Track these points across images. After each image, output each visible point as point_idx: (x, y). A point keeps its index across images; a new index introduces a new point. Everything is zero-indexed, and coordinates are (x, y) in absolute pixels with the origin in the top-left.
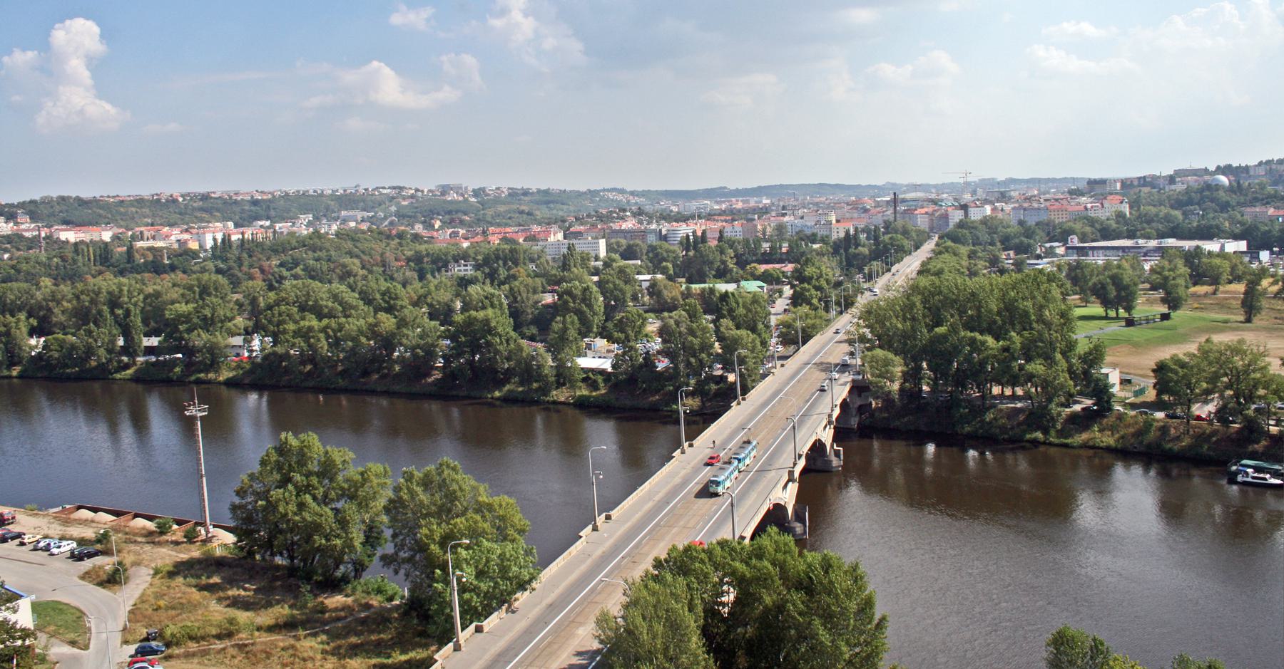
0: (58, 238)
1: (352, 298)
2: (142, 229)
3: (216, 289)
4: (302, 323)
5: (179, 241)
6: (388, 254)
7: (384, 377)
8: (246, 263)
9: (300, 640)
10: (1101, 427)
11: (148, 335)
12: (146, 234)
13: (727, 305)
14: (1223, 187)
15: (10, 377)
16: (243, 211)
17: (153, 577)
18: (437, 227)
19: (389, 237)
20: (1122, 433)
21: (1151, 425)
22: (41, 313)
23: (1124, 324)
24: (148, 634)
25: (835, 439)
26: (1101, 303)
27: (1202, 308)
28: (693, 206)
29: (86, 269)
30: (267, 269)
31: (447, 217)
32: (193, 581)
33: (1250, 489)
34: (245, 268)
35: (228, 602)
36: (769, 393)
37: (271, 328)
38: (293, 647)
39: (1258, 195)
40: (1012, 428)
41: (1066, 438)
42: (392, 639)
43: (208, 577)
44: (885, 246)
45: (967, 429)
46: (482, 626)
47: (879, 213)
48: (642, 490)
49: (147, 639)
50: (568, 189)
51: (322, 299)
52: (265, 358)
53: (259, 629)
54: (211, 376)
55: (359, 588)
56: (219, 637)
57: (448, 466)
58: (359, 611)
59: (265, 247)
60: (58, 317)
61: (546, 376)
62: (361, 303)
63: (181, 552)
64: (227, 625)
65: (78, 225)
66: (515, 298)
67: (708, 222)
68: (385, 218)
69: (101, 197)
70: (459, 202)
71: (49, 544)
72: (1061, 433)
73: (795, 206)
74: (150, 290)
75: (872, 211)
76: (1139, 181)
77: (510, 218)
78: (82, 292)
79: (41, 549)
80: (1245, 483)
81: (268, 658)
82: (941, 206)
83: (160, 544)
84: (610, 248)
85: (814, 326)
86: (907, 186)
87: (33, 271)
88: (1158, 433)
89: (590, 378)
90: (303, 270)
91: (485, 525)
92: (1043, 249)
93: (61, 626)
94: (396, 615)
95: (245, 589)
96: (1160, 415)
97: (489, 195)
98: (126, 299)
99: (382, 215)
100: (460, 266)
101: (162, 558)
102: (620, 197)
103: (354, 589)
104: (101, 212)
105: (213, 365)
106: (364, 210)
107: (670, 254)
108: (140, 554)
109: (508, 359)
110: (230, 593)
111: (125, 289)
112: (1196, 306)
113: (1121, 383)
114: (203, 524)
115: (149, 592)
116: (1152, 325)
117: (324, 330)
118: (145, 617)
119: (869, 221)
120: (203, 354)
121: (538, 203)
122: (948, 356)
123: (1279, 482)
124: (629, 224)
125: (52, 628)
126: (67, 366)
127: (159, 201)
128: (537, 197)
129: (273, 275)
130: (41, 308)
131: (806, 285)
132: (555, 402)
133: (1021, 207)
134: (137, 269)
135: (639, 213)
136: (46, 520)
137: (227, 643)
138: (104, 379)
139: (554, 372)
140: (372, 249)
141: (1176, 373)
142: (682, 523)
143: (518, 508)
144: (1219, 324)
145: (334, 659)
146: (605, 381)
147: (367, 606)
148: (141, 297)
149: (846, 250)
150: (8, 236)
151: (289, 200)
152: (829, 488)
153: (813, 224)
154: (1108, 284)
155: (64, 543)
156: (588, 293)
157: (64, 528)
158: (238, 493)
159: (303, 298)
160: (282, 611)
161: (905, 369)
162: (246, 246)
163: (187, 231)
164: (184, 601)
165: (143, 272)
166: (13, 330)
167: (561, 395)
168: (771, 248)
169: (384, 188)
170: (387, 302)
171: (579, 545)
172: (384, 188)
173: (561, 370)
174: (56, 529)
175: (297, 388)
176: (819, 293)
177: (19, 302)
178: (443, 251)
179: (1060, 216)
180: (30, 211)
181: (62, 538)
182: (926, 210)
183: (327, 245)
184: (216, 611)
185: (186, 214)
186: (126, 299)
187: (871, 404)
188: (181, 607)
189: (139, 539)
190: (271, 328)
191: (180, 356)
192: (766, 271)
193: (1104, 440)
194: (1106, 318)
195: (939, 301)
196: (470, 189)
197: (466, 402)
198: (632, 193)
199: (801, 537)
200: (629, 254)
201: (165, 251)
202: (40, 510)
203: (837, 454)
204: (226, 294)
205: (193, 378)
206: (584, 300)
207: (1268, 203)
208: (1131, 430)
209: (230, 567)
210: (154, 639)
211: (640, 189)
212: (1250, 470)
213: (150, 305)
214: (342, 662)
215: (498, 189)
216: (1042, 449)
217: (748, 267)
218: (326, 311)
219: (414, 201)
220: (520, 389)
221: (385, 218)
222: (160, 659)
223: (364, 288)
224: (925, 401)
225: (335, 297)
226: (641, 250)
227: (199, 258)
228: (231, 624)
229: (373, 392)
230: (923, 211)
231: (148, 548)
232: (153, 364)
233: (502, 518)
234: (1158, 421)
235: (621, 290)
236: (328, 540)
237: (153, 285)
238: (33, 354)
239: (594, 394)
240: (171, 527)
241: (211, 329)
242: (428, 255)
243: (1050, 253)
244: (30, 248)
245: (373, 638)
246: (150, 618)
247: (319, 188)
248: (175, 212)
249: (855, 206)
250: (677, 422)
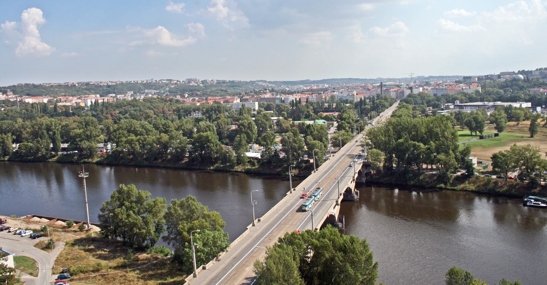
0: (25, 101)
1: (150, 127)
3: (92, 123)
4: (129, 138)
5: (76, 103)
6: (165, 108)
7: (163, 160)
8: (105, 112)
9: (128, 272)
10: (469, 182)
11: (63, 143)
12: (62, 100)
13: (310, 130)
14: (521, 80)
15: (4, 161)
16: (103, 90)
17: (65, 246)
18: (186, 97)
19: (166, 101)
20: (478, 184)
21: (490, 181)
22: (18, 133)
23: (479, 138)
24: (63, 270)
25: (356, 187)
26: (469, 129)
27: (512, 131)
28: (295, 88)
29: (37, 115)
30: (114, 114)
31: (190, 92)
32: (82, 247)
33: (532, 208)
34: (104, 114)
35: (97, 256)
36: (328, 168)
37: (116, 140)
38: (125, 275)
39: (536, 83)
40: (431, 182)
41: (454, 186)
42: (167, 272)
43: (89, 246)
44: (377, 105)
45: (412, 183)
46: (205, 267)
47: (375, 91)
48: (273, 209)
49: (63, 272)
50: (242, 80)
51: (137, 127)
52: (113, 152)
53: (110, 268)
54: (90, 160)
55: (153, 250)
56: (93, 271)
57: (191, 199)
58: (153, 260)
59: (113, 105)
60: (25, 135)
61: (233, 160)
62: (154, 129)
63: (77, 235)
64: (97, 266)
65: (33, 96)
66: (219, 127)
67: (302, 95)
68: (164, 93)
69: (43, 84)
70: (195, 86)
71: (21, 232)
72: (452, 185)
73: (339, 88)
74: (64, 123)
75: (371, 90)
76: (485, 77)
77: (217, 93)
78: (35, 125)
79: (18, 234)
80: (530, 206)
81: (114, 280)
82: (401, 88)
83: (68, 232)
84: (260, 106)
85: (347, 139)
86: (386, 79)
87: (14, 115)
88: (493, 185)
89: (251, 161)
90: (129, 115)
91: (207, 224)
92: (444, 106)
93: (26, 267)
94: (169, 262)
95: (104, 251)
96: (494, 177)
97: (208, 83)
98: (54, 127)
99: (163, 92)
100: (196, 113)
101: (69, 238)
102: (264, 84)
103: (151, 251)
104: (43, 90)
105: (91, 155)
106: (155, 89)
107: (286, 108)
108: (59, 236)
109: (217, 153)
110: (98, 253)
111: (53, 123)
112: (510, 130)
113: (478, 163)
114: (86, 223)
115: (63, 252)
116: (491, 138)
117: (138, 141)
118: (62, 263)
120: (87, 151)
121: (229, 86)
122: (404, 152)
123: (545, 205)
124: (268, 95)
125: (22, 268)
126: (28, 156)
127: (68, 85)
128: (229, 84)
129: (116, 117)
130: (17, 131)
131: (343, 122)
132: (236, 171)
133: (435, 88)
134: (58, 115)
135: (272, 91)
136: (20, 221)
137: (97, 274)
138: (44, 161)
139: (236, 159)
140: (158, 106)
141: (501, 159)
142: (290, 223)
143: (221, 217)
144: (519, 138)
145: (142, 281)
146: (258, 162)
147: (157, 258)
148: (60, 126)
149: (360, 107)
150: (4, 101)
151: (123, 85)
152: (353, 208)
153: (346, 95)
154: (472, 121)
155: (27, 231)
156: (250, 125)
157: (27, 225)
158: (101, 210)
159: (129, 127)
160: (120, 260)
161: (385, 157)
162: (105, 105)
163: (79, 98)
164: (78, 256)
165: (61, 116)
166: (6, 141)
167: (239, 168)
168: (329, 106)
169: (163, 80)
170: (165, 129)
171: (247, 232)
172: (163, 80)
173: (239, 158)
174: (24, 226)
175: (127, 165)
176: (349, 125)
177: (8, 129)
178: (189, 107)
179: (452, 92)
180: (13, 90)
181: (26, 229)
182: (394, 89)
183: (140, 104)
184: (92, 260)
185: (79, 91)
186: (54, 127)
187: (371, 172)
188: (77, 258)
189: (59, 230)
190: (116, 140)
191: (77, 151)
192: (326, 115)
193: (470, 187)
194: (471, 135)
195: (400, 128)
196: (200, 80)
197: (198, 171)
198: (269, 82)
199: (341, 229)
200: (268, 108)
201: (70, 107)
202: (17, 217)
203: (357, 193)
204: (96, 125)
205: (82, 161)
206: (249, 128)
207: (540, 86)
208: (482, 183)
209: (98, 241)
210: (66, 272)
211: (273, 81)
212: (532, 200)
213: (64, 130)
214: (146, 282)
215: (212, 80)
216: (444, 191)
217: (319, 114)
218: (139, 132)
219: (176, 86)
220: (222, 166)
221: (164, 93)
222: (68, 281)
223: (155, 123)
224: (394, 171)
225: (143, 127)
226: (273, 107)
228: (98, 266)
229: (159, 167)
230: (393, 90)
231: (63, 233)
232: (65, 155)
233: (214, 221)
234: (493, 179)
235: (265, 124)
236: (140, 230)
237: (65, 121)
238: (14, 151)
239: (253, 168)
240: (73, 224)
241: (90, 140)
242: (182, 109)
243: (447, 108)
244: (13, 106)
245: (159, 272)
247: (136, 80)
248: (75, 91)
249: (364, 88)
250: (289, 180)
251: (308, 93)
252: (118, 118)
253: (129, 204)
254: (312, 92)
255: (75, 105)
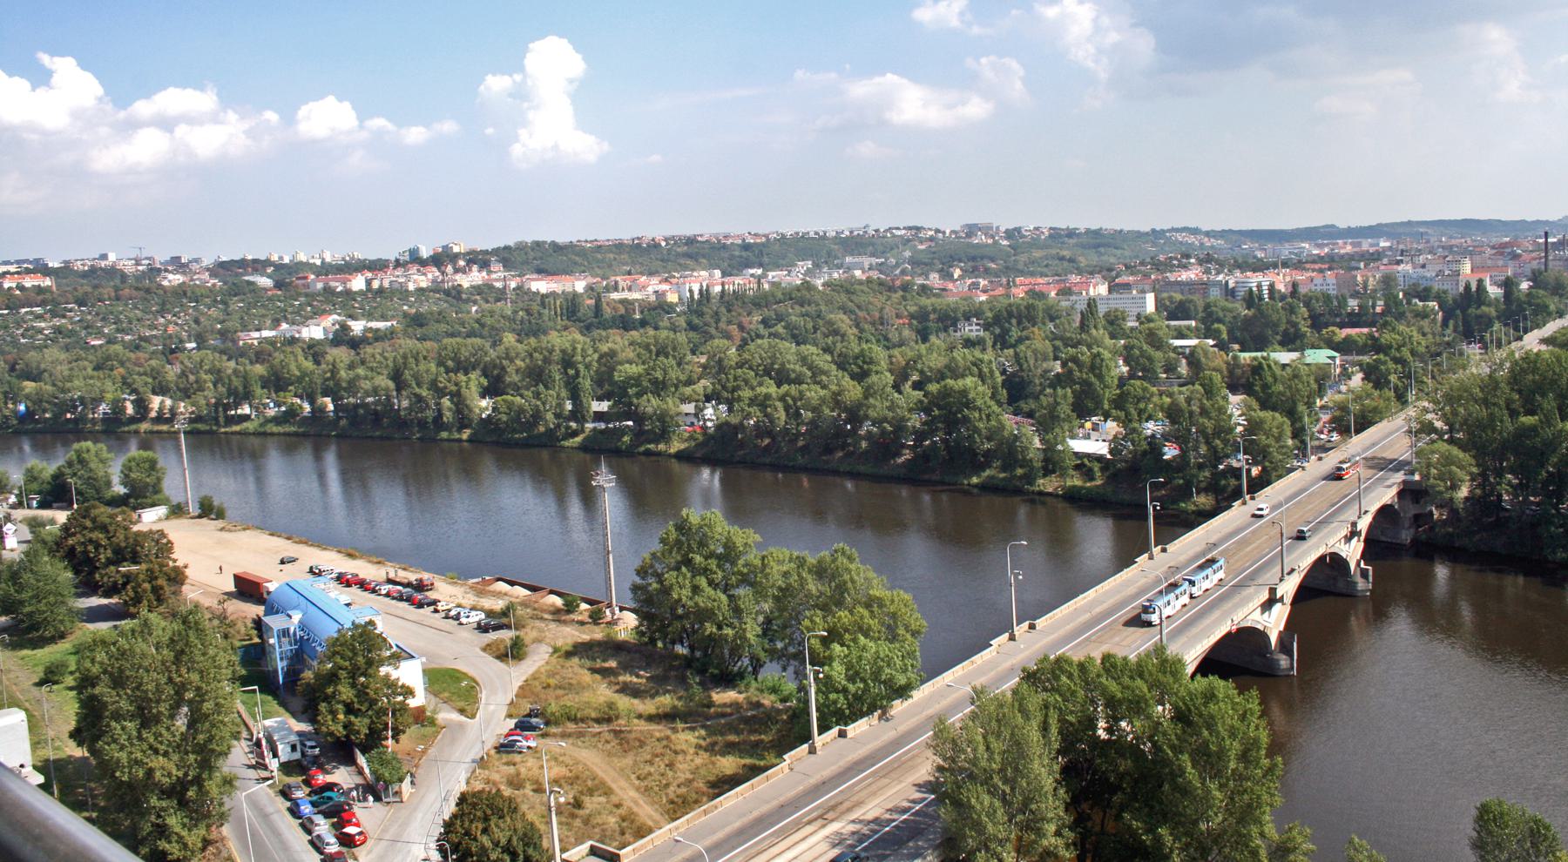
0: (529, 289)
1: (824, 361)
2: (618, 279)
3: (674, 349)
4: (758, 390)
5: (656, 292)
6: (887, 310)
7: (849, 455)
8: (724, 319)
9: (678, 732)
11: (600, 399)
12: (622, 284)
15: (460, 440)
16: (732, 257)
17: (551, 656)
18: (956, 276)
19: (891, 289)
22: (495, 372)
24: (531, 710)
25: (1365, 555)
28: (1286, 251)
29: (551, 324)
30: (746, 325)
31: (970, 264)
32: (588, 663)
35: (617, 687)
36: (1293, 490)
37: (725, 394)
38: (668, 738)
42: (771, 741)
43: (604, 660)
46: (845, 731)
47: (1535, 259)
48: (1085, 598)
49: (529, 715)
50: (1126, 228)
51: (789, 362)
52: (719, 427)
53: (640, 716)
54: (662, 447)
55: (754, 684)
56: (598, 721)
57: (843, 553)
58: (747, 710)
59: (746, 300)
60: (513, 377)
61: (1031, 460)
62: (834, 367)
63: (584, 633)
64: (606, 709)
65: (554, 274)
66: (1021, 365)
67: (1294, 272)
68: (897, 265)
69: (579, 241)
70: (987, 245)
71: (459, 613)
74: (604, 348)
75: (1523, 258)
77: (1047, 266)
78: (535, 350)
79: (452, 618)
81: (641, 747)
83: (565, 622)
84: (1159, 304)
85: (1375, 410)
87: (498, 326)
90: (784, 328)
91: (871, 622)
93: (454, 693)
94: (785, 717)
95: (638, 676)
97: (1025, 237)
98: (579, 358)
99: (893, 261)
100: (970, 325)
101: (564, 637)
102: (1191, 239)
103: (748, 686)
104: (577, 258)
105: (664, 435)
106: (873, 255)
108: (544, 632)
109: (989, 439)
110: (621, 678)
111: (579, 347)
114: (610, 606)
115: (543, 670)
117: (782, 399)
118: (533, 693)
119: (1519, 271)
120: (653, 423)
121: (1083, 246)
122: (1541, 456)
124: (1191, 274)
125: (446, 694)
126: (514, 431)
127: (639, 245)
128: (1084, 240)
129: (748, 333)
130: (495, 366)
131: (1381, 356)
132: (1041, 493)
134: (604, 325)
136: (462, 589)
137: (605, 728)
138: (551, 446)
139: (1042, 456)
140: (870, 303)
142: (1117, 639)
143: (915, 606)
145: (706, 755)
146: (1103, 470)
147: (758, 705)
148: (596, 356)
149: (1464, 311)
150: (479, 286)
151: (785, 243)
152: (1353, 618)
153: (1434, 275)
155: (473, 613)
156: (1098, 361)
157: (477, 599)
158: (638, 573)
159: (769, 361)
160: (666, 701)
162: (726, 298)
163: (666, 280)
164: (573, 682)
165: (611, 327)
166: (463, 390)
167: (1048, 484)
169: (898, 229)
170: (861, 367)
171: (987, 654)
172: (898, 229)
173: (1049, 454)
174: (470, 599)
175: (754, 465)
176: (1399, 366)
177: (473, 360)
178: (952, 306)
180: (503, 258)
181: (473, 608)
183: (817, 297)
184: (603, 693)
185: (668, 260)
186: (579, 358)
187: (1431, 513)
188: (568, 687)
189: (546, 616)
190: (725, 394)
191: (630, 423)
196: (1003, 229)
197: (939, 488)
198: (1208, 234)
199: (1286, 673)
200: (1178, 311)
201: (637, 304)
202: (459, 579)
203: (1364, 574)
204: (685, 355)
205: (642, 449)
206: (1092, 368)
209: (629, 652)
210: (536, 716)
211: (1219, 228)
213: (605, 366)
214: (713, 758)
215: (1037, 229)
217: (1324, 331)
218: (793, 376)
219: (933, 244)
220: (1002, 475)
221: (897, 265)
222: (538, 736)
223: (844, 350)
224: (1507, 514)
225: (804, 360)
226: (1195, 307)
227: (675, 311)
228: (611, 708)
229: (836, 472)
231: (553, 626)
232: (602, 432)
233: (894, 616)
235: (1150, 359)
236: (720, 628)
237: (616, 341)
238: (484, 416)
239: (1088, 484)
240: (578, 606)
241: (662, 393)
242: (934, 310)
244: (498, 300)
245: (752, 738)
246: (537, 695)
247: (820, 229)
248: (657, 259)
249: (1500, 249)
251: (1317, 266)
252: (753, 334)
253: (702, 560)
254: (1331, 261)
255: (653, 298)
